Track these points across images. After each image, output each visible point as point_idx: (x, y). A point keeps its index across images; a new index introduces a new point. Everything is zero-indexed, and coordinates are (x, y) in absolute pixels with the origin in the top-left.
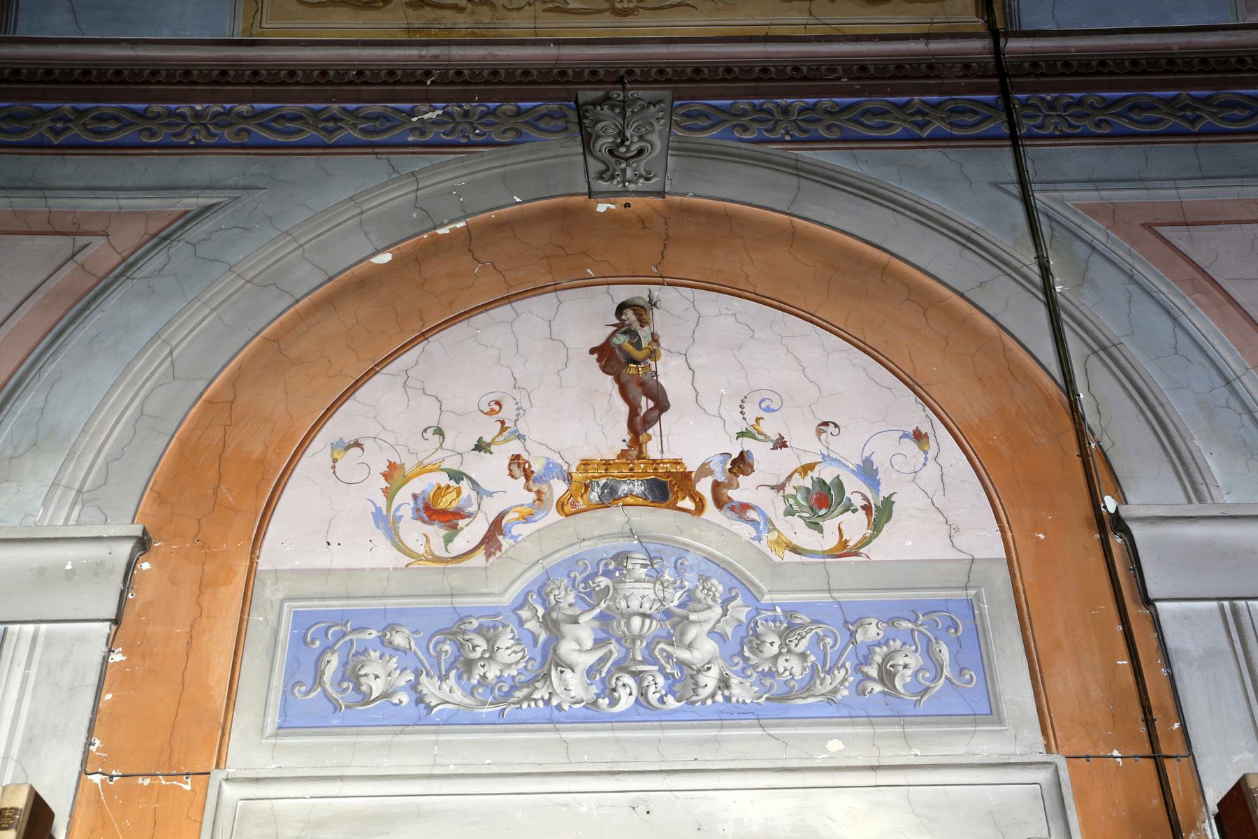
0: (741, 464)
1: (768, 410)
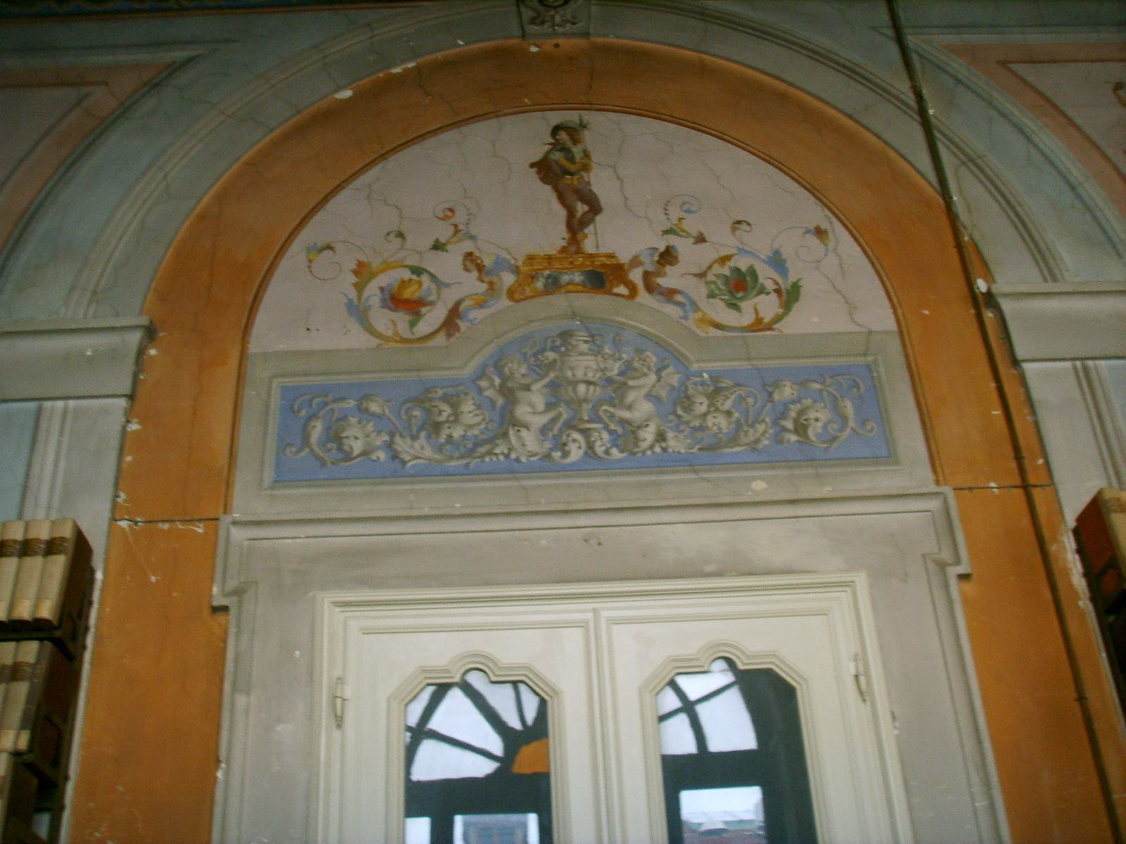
0: (668, 257)
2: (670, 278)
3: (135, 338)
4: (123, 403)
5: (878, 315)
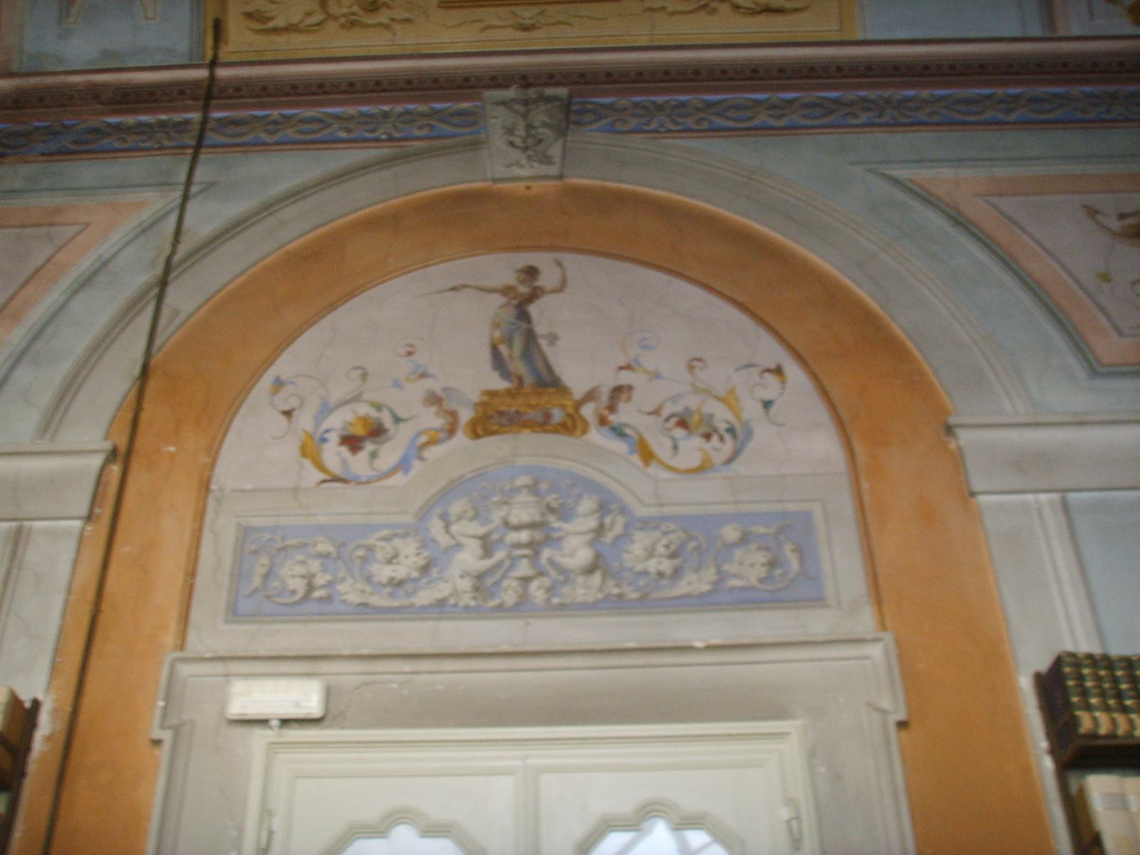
0: (619, 392)
1: (646, 347)
2: (626, 414)
3: (97, 461)
4: (77, 524)
5: (820, 446)
